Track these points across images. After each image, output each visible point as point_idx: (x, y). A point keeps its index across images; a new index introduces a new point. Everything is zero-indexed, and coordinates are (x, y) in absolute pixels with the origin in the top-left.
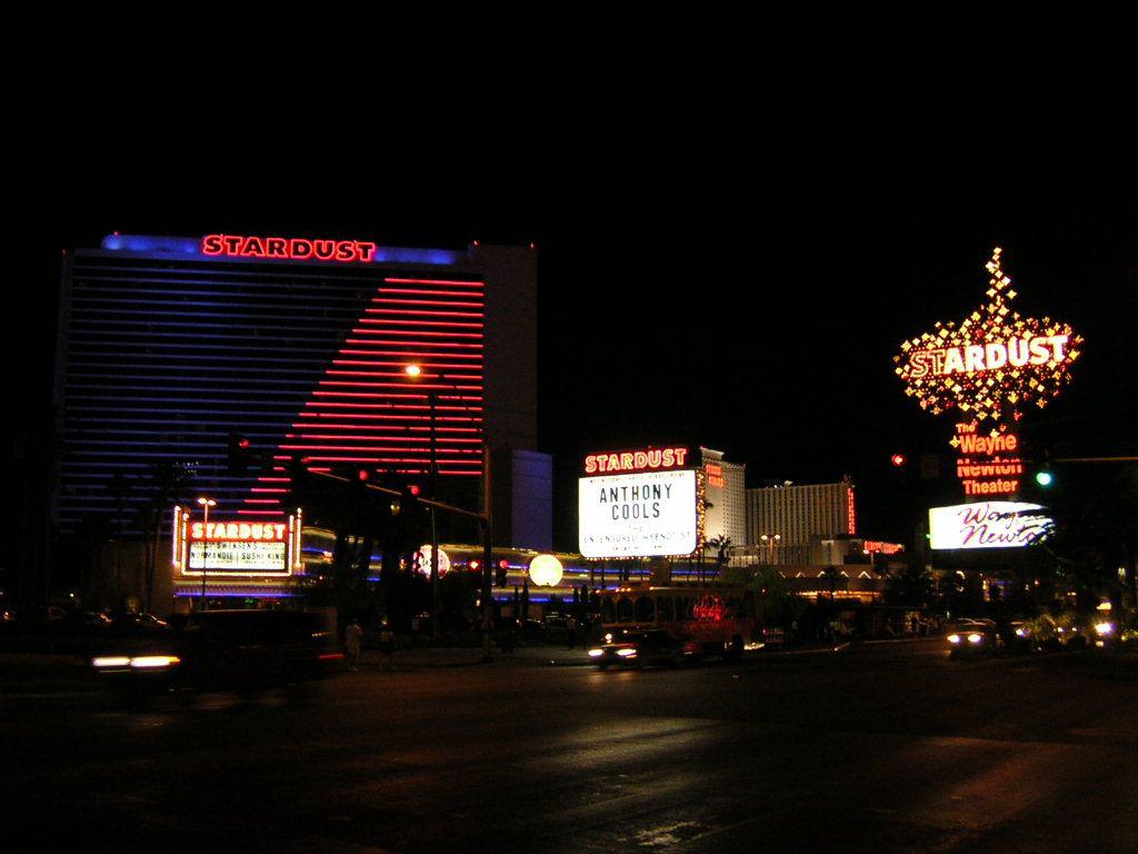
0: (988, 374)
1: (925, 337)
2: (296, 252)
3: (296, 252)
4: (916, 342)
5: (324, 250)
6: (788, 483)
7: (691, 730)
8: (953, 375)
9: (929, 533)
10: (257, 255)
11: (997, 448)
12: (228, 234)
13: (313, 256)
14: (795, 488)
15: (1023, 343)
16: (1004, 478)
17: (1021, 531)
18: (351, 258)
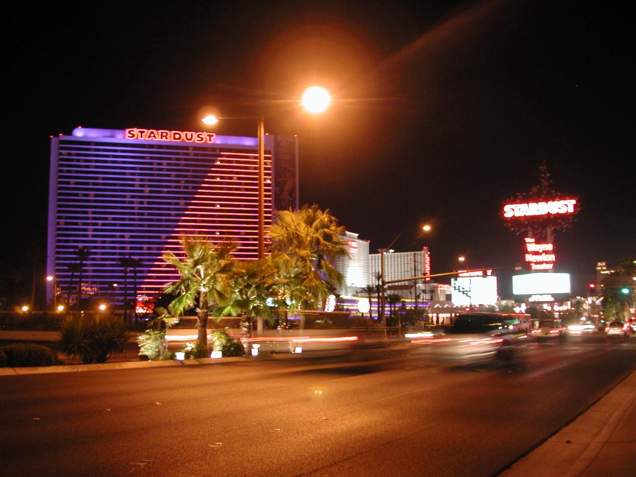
2: (175, 139)
3: (175, 139)
5: (189, 137)
6: (391, 251)
7: (349, 349)
9: (82, 127)
10: (155, 139)
12: (139, 128)
13: (183, 141)
14: (396, 254)
16: (547, 263)
18: (202, 142)
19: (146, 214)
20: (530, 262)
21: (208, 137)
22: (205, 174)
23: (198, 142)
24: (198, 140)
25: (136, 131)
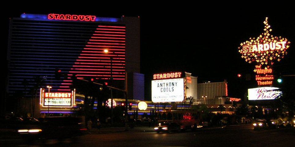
0: (264, 52)
1: (247, 42)
2: (74, 19)
3: (74, 19)
4: (244, 43)
6: (209, 82)
8: (255, 52)
10: (63, 19)
13: (79, 20)
14: (211, 83)
15: (274, 43)
16: (269, 80)
17: (273, 95)
20: (256, 73)
21: (92, 18)
22: (61, 81)
23: (50, 19)
24: (86, 20)
25: (53, 15)
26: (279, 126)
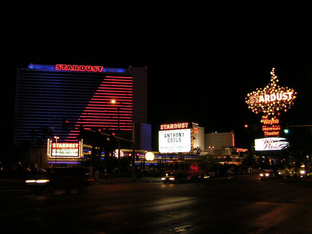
0: (271, 102)
1: (254, 92)
2: (81, 69)
3: (81, 69)
4: (251, 94)
5: (89, 69)
6: (216, 132)
7: (189, 200)
8: (261, 103)
9: (255, 146)
10: (71, 70)
11: (273, 123)
12: (62, 64)
13: (86, 70)
14: (218, 134)
15: (281, 94)
16: (275, 131)
17: (280, 146)
18: (96, 71)
19: (89, 86)
21: (63, 67)
26: (285, 176)
